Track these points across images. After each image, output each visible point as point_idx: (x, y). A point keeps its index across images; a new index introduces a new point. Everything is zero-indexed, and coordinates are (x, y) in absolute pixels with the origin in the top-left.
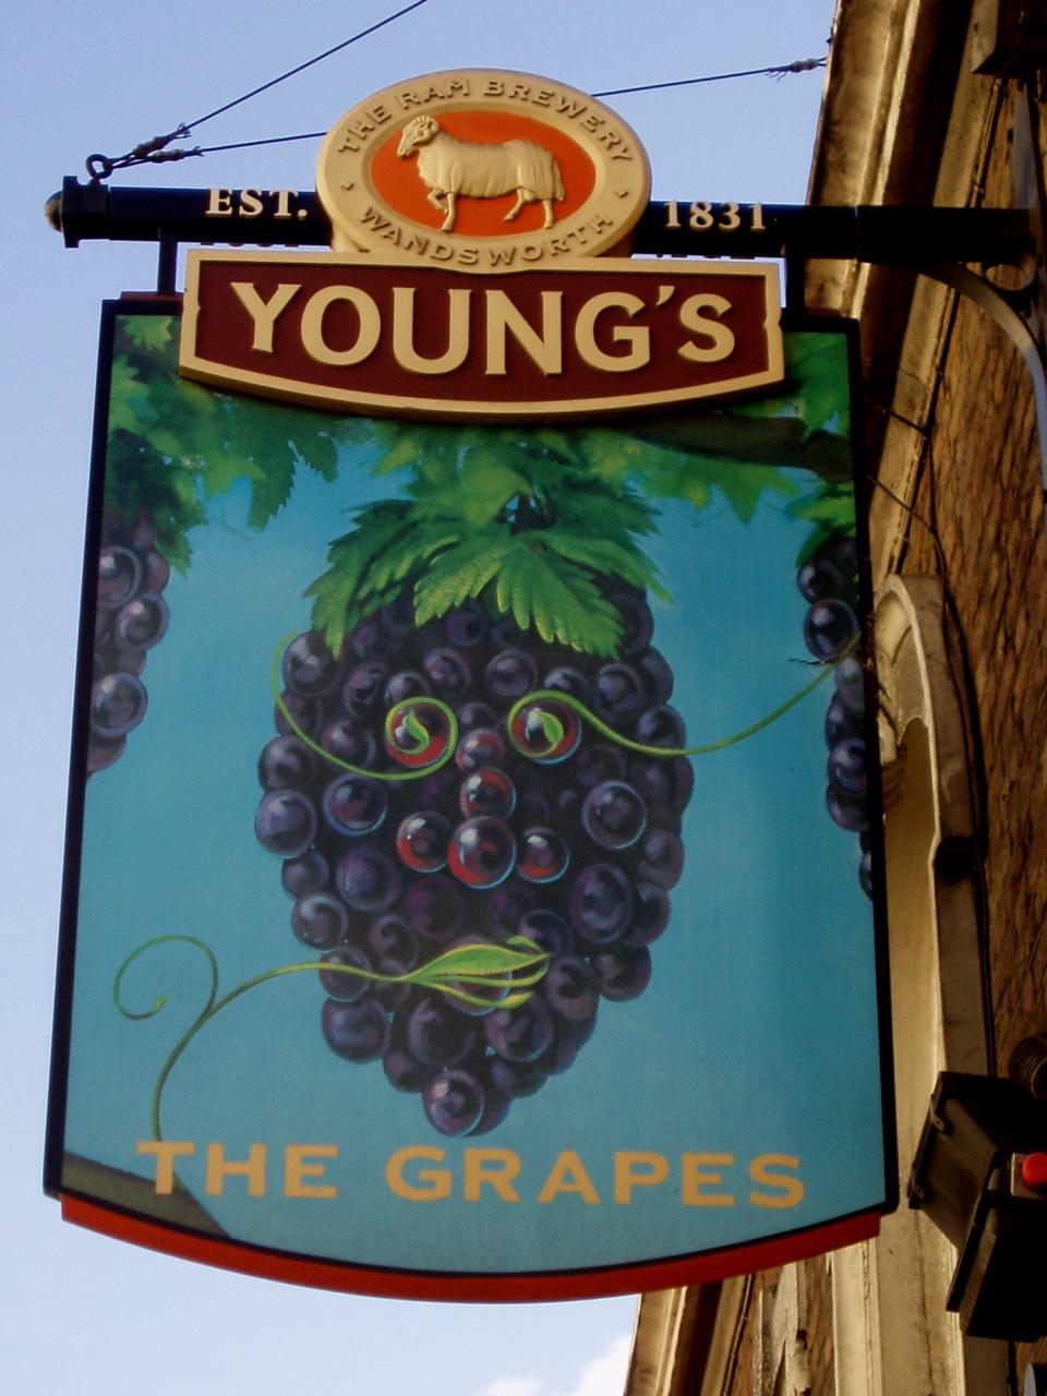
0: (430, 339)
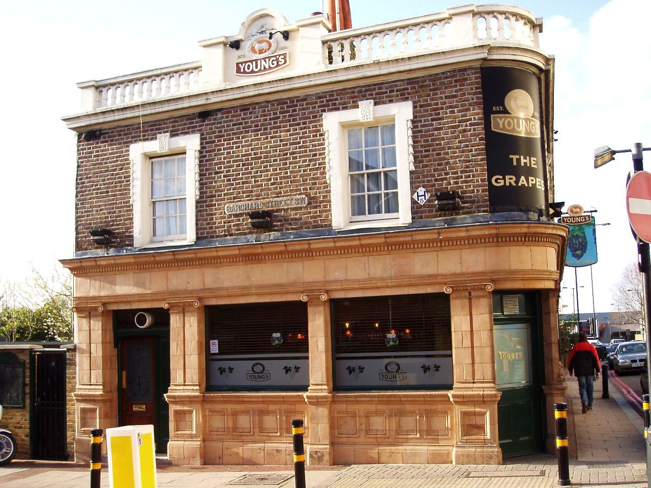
0: (574, 221)
